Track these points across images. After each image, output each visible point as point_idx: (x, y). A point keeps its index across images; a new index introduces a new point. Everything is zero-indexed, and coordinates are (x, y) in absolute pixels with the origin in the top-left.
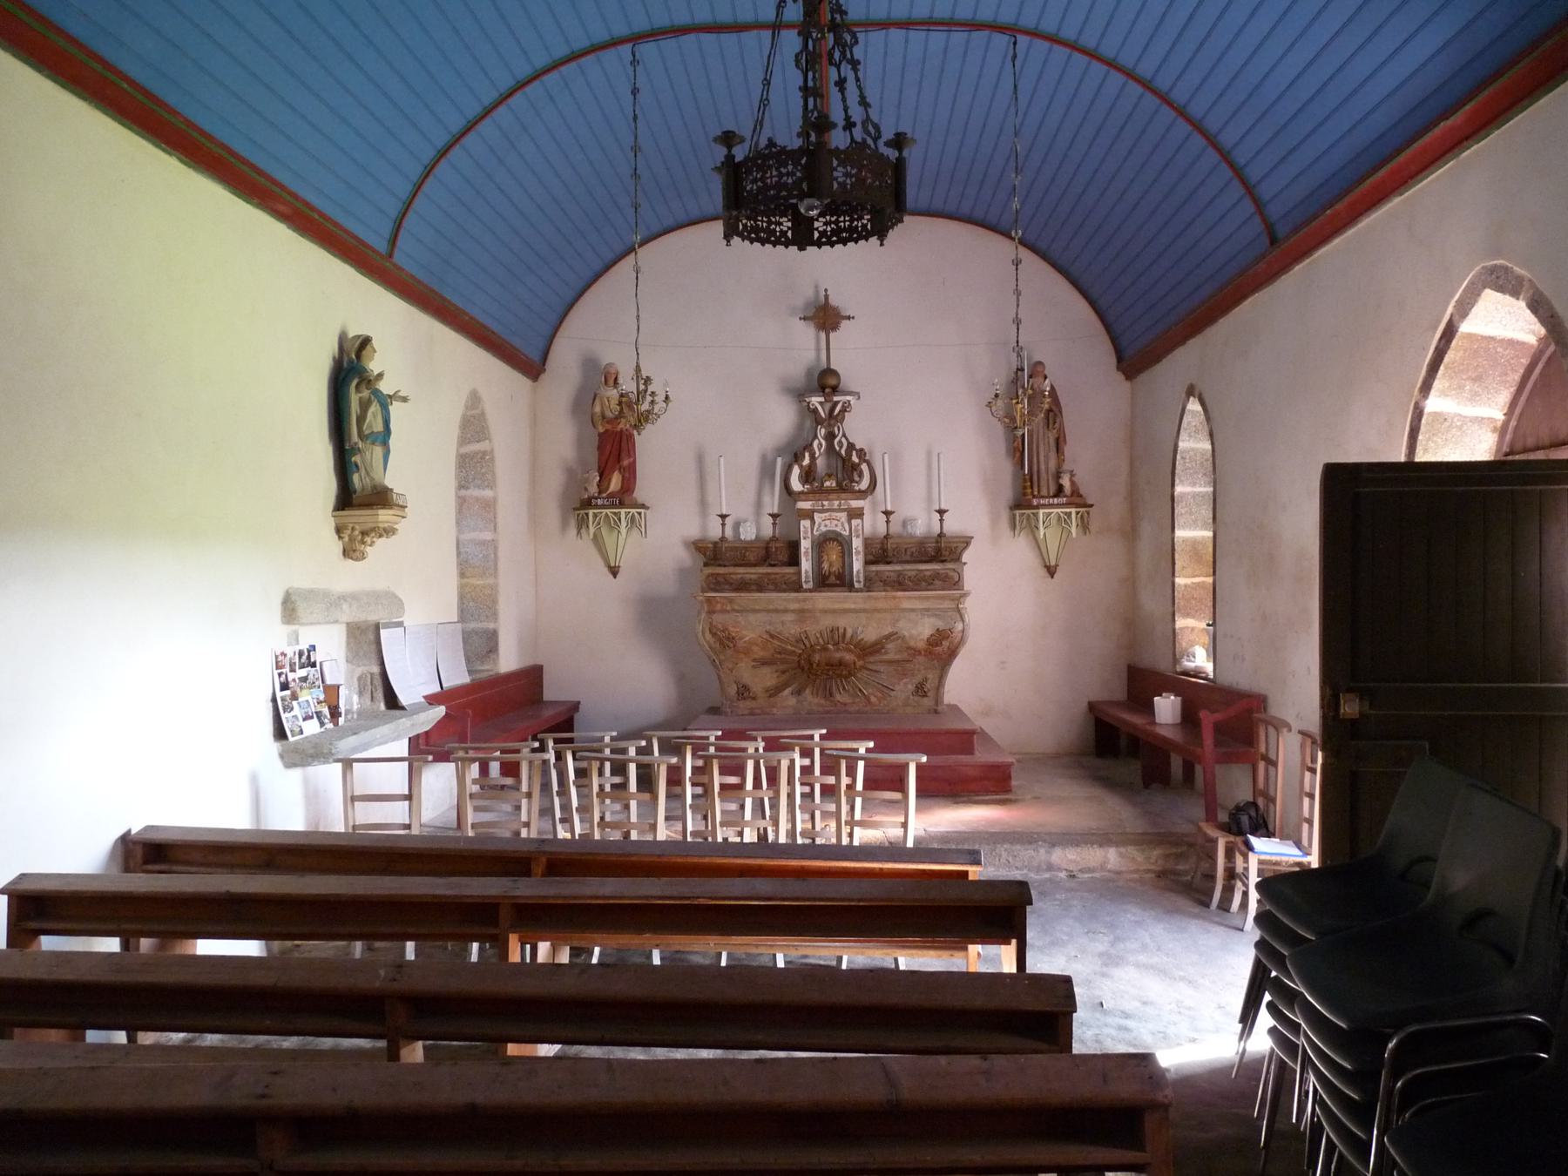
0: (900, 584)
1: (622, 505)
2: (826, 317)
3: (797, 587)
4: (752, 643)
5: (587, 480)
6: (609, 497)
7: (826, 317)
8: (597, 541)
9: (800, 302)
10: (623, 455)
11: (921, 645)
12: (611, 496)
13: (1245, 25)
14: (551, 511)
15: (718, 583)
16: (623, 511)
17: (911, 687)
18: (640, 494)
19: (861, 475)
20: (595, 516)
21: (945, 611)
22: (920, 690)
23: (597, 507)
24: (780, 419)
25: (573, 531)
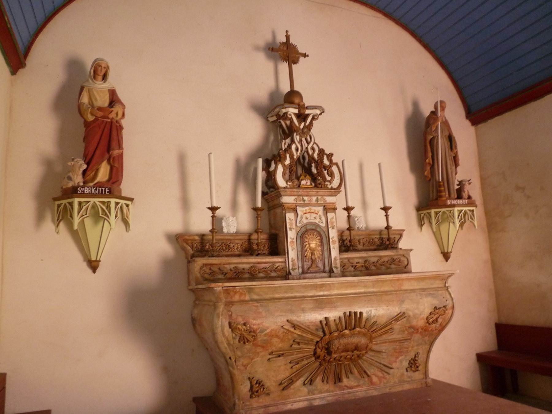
0: (367, 268)
1: (111, 194)
2: (286, 53)
3: (286, 275)
4: (273, 335)
5: (72, 169)
7: (286, 53)
9: (262, 43)
11: (421, 323)
13: (401, 5)
15: (213, 273)
16: (113, 201)
17: (406, 364)
18: (126, 188)
19: (331, 175)
21: (436, 289)
22: (413, 364)
23: (83, 195)
24: (251, 132)
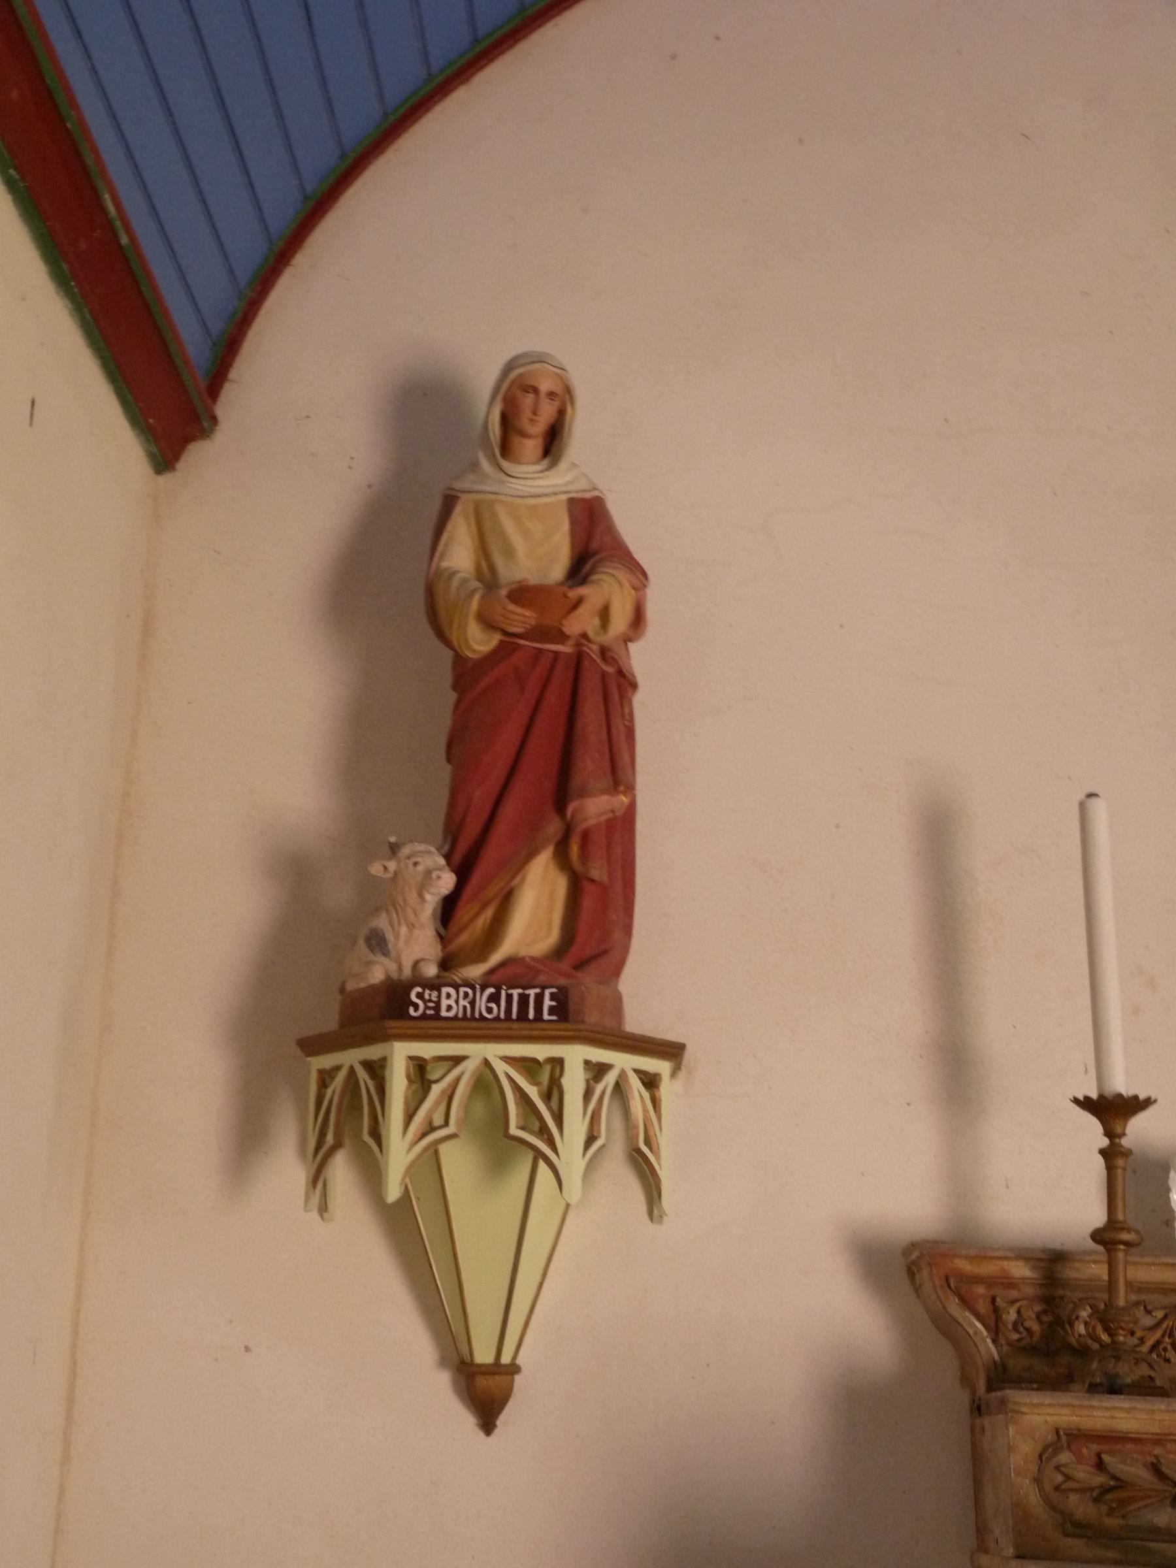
1: (567, 1019)
5: (381, 897)
6: (495, 980)
8: (415, 1236)
10: (589, 764)
12: (516, 972)
14: (187, 1072)
16: (576, 1056)
18: (648, 989)
20: (420, 1070)
23: (435, 1026)
25: (284, 1169)
